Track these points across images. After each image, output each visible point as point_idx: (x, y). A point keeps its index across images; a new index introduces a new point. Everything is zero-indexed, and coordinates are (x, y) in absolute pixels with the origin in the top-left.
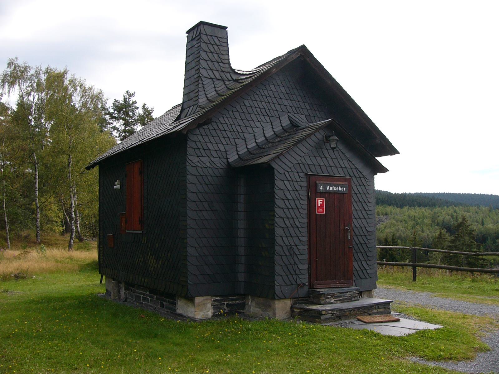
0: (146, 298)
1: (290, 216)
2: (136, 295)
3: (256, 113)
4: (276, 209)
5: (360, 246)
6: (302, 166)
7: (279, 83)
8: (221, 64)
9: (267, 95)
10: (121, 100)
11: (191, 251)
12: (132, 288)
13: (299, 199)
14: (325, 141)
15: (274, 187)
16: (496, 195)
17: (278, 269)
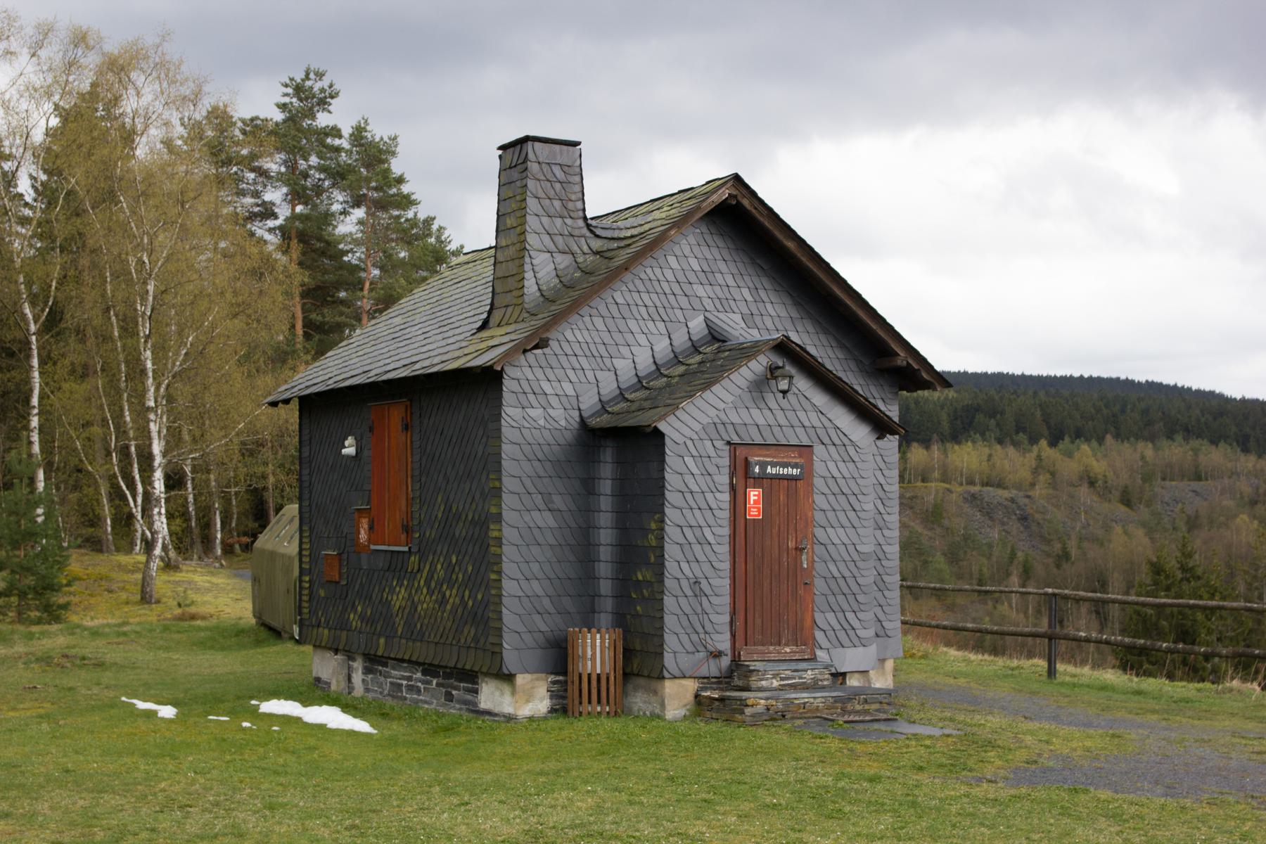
0: (412, 686)
1: (693, 523)
2: (391, 683)
3: (639, 317)
4: (667, 510)
5: (841, 582)
6: (720, 427)
7: (687, 251)
8: (569, 221)
9: (661, 278)
11: (508, 586)
12: (380, 668)
13: (714, 490)
14: (769, 376)
15: (663, 470)
17: (669, 621)
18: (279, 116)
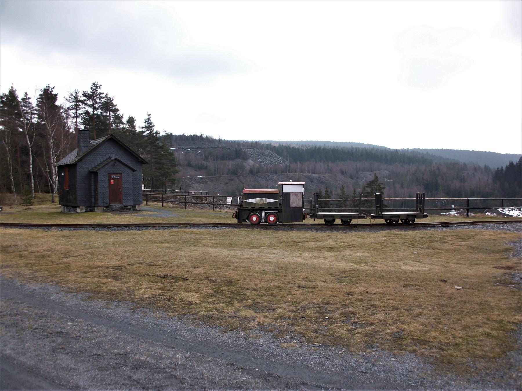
10: (89, 91)
16: (508, 153)
18: (36, 123)
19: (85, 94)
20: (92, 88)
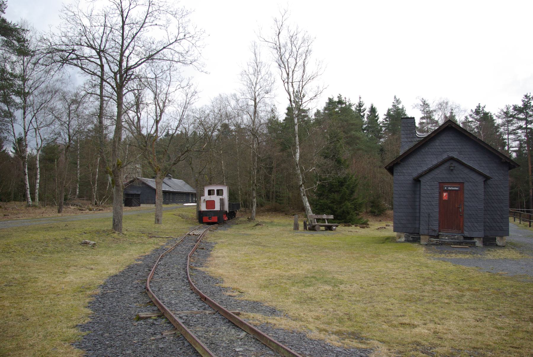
10: (520, 104)
19: (515, 108)
20: (523, 101)
